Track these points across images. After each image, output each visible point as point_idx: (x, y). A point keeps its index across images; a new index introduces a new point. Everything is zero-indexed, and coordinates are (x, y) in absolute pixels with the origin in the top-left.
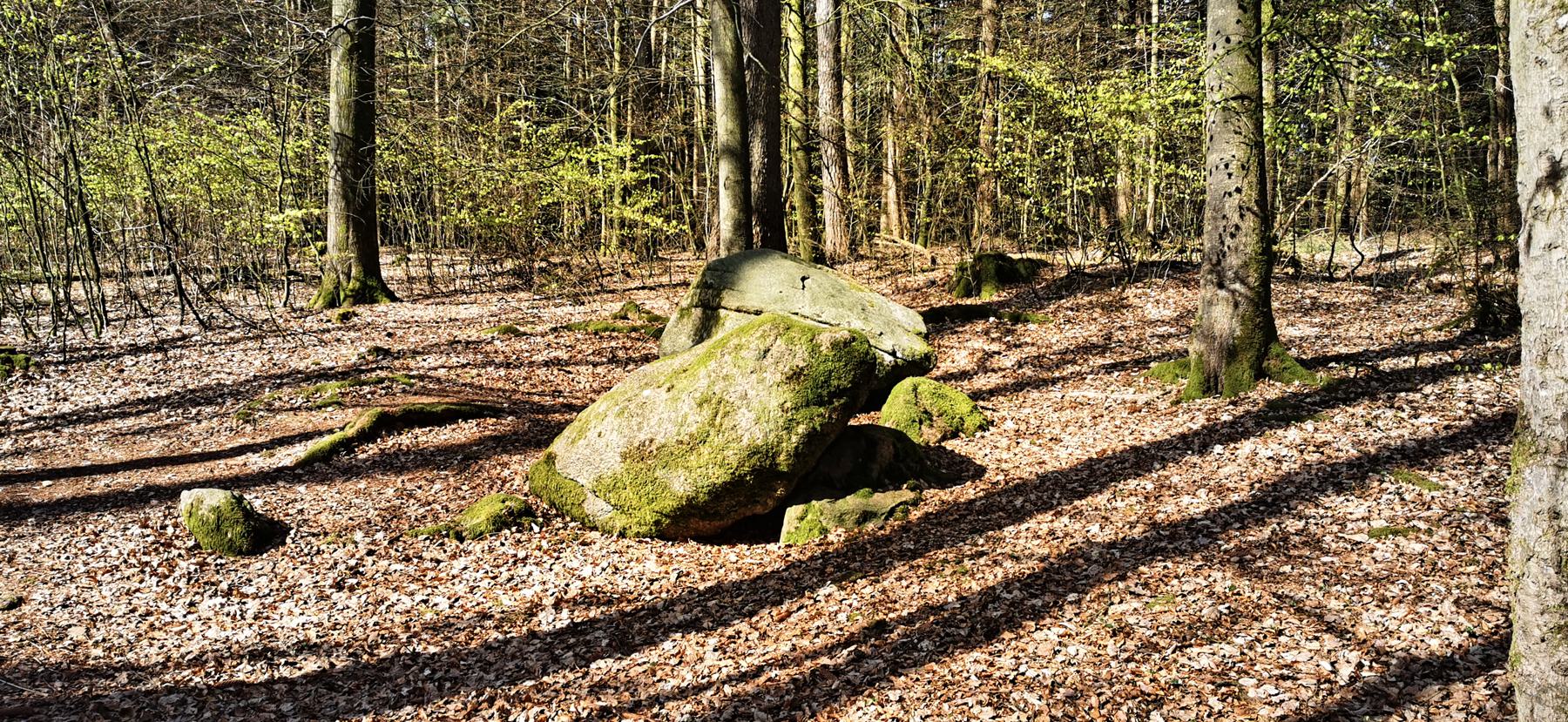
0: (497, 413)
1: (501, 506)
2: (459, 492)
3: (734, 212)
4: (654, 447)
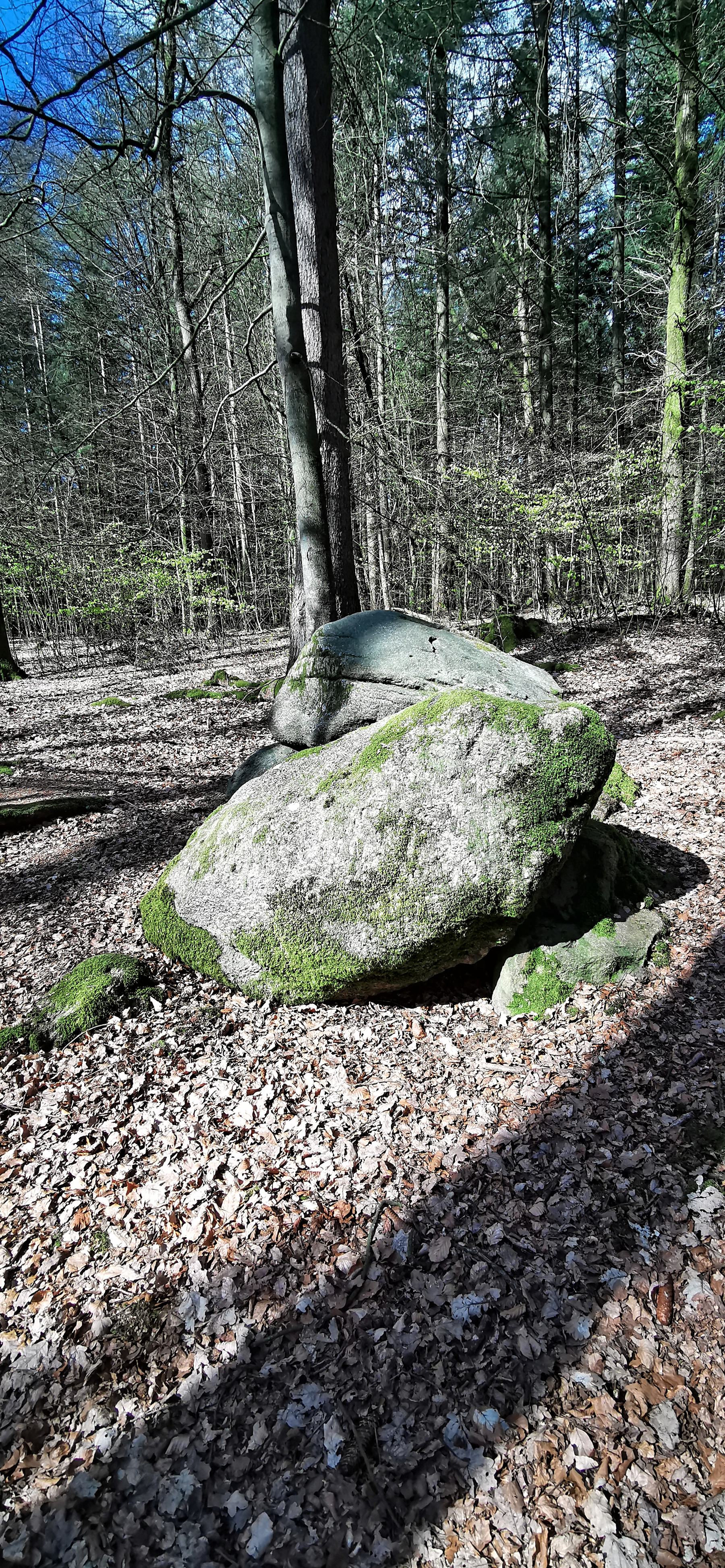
0: (101, 806)
1: (103, 979)
2: (50, 947)
3: (318, 581)
4: (316, 890)
